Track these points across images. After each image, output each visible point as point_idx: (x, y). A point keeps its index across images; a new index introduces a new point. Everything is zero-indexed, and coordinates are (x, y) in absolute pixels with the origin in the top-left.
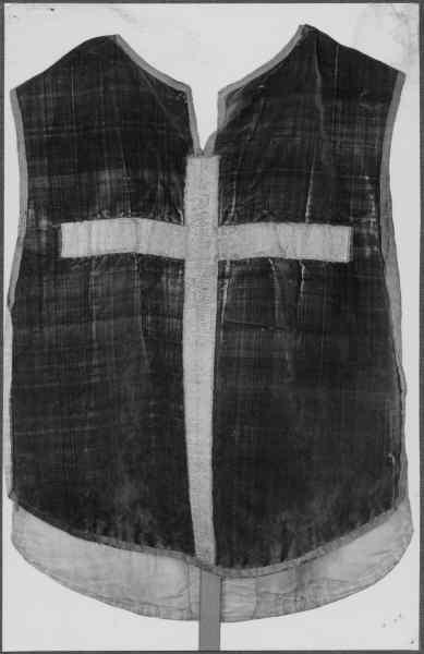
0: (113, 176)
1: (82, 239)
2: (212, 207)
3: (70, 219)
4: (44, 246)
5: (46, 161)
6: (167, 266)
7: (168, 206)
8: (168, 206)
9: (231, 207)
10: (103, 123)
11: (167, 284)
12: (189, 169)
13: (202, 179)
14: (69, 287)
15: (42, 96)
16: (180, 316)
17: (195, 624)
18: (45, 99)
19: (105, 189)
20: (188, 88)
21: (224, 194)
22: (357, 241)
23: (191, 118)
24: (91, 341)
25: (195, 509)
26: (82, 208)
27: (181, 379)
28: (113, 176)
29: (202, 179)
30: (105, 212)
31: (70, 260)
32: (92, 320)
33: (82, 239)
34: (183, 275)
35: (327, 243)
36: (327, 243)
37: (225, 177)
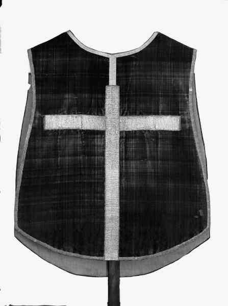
0: (70, 96)
1: (54, 122)
2: (117, 107)
3: (48, 114)
4: (37, 124)
5: (40, 88)
6: (97, 134)
7: (98, 108)
8: (98, 108)
9: (125, 108)
10: (62, 71)
11: (98, 142)
12: (107, 92)
13: (112, 95)
14: (48, 143)
15: (41, 60)
16: (103, 154)
17: (107, 278)
18: (42, 61)
19: (67, 102)
20: (17, 235)
21: (122, 102)
22: (183, 122)
23: (193, 56)
24: (58, 166)
25: (108, 195)
26: (56, 110)
27: (103, 240)
28: (70, 96)
29: (112, 95)
30: (65, 112)
31: (48, 130)
32: (58, 157)
33: (54, 122)
34: (104, 137)
35: (169, 123)
36: (169, 123)
37: (122, 96)
